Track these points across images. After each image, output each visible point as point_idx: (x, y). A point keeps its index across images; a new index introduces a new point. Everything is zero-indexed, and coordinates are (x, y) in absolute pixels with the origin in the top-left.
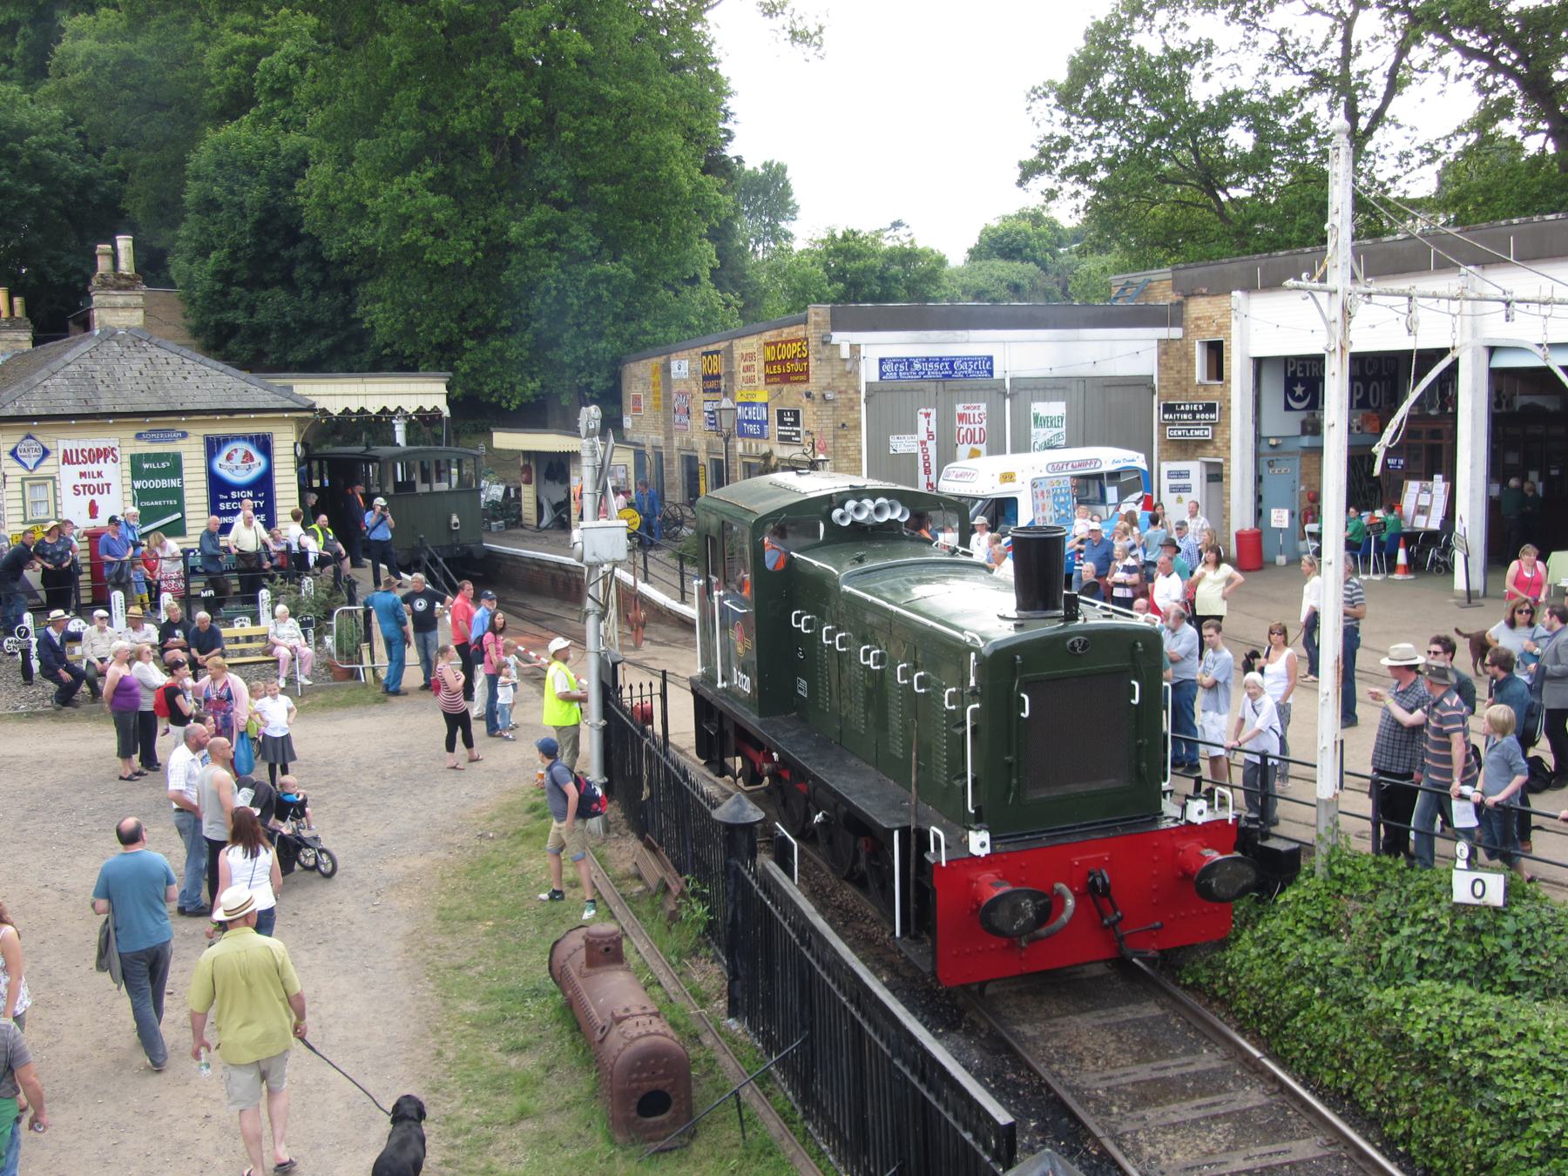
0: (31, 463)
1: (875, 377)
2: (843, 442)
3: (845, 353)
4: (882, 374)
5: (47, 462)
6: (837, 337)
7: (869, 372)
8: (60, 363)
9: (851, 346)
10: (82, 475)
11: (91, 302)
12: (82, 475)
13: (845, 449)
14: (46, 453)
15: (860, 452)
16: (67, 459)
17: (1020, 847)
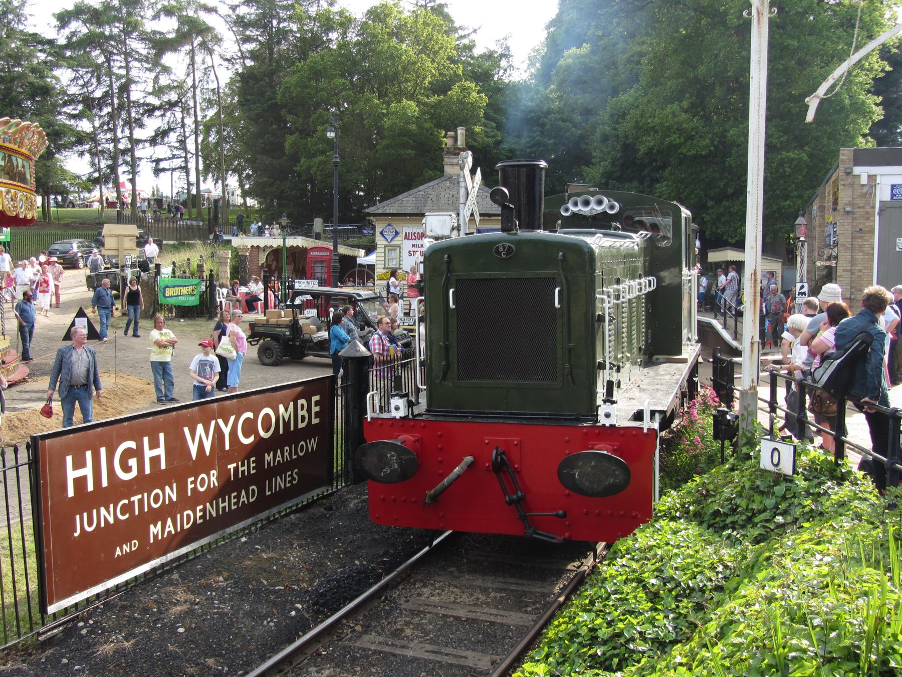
0: (389, 238)
1: (887, 197)
2: (860, 241)
3: (864, 180)
4: (893, 195)
5: (398, 238)
6: (857, 170)
7: (883, 194)
8: (416, 190)
9: (869, 176)
10: (413, 246)
11: (443, 160)
12: (413, 246)
13: (861, 246)
14: (397, 233)
15: (873, 249)
16: (407, 237)
17: (433, 419)
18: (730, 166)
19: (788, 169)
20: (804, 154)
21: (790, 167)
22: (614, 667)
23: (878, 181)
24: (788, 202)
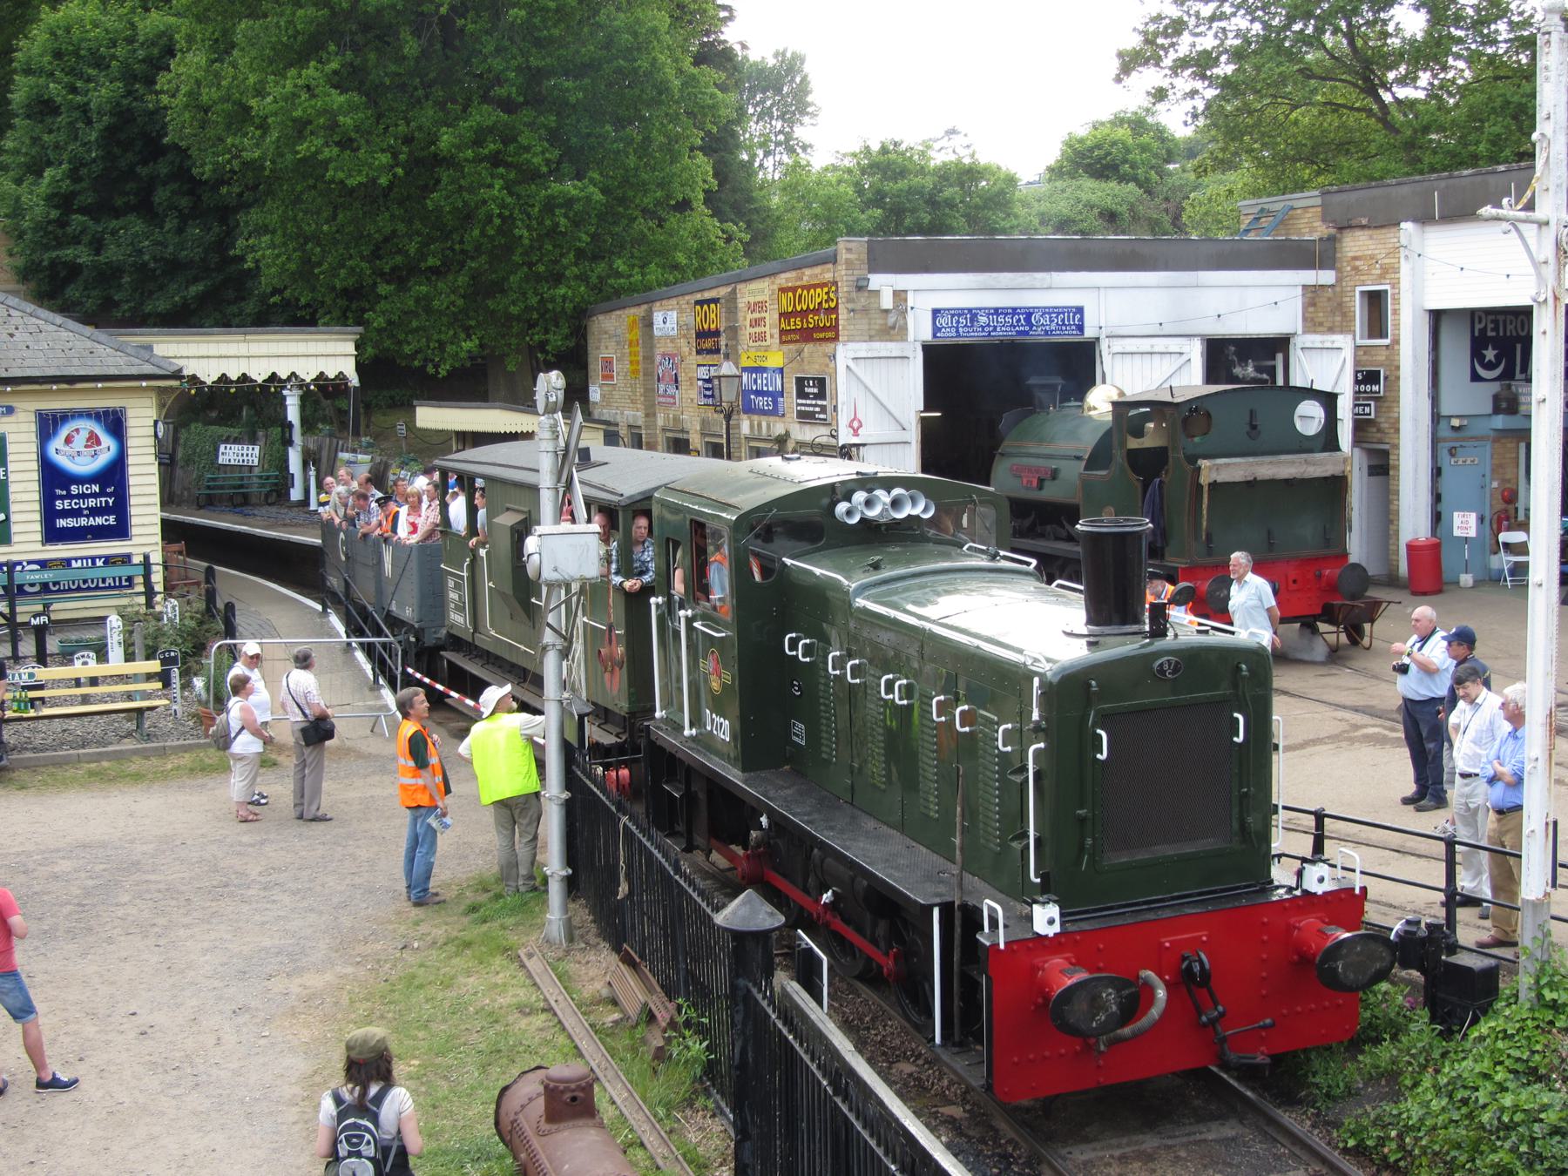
3: (887, 302)
6: (877, 281)
9: (896, 294)
18: (439, 209)
19: (563, 221)
20: (592, 189)
21: (566, 216)
22: (741, 982)
23: (910, 304)
24: (562, 291)
